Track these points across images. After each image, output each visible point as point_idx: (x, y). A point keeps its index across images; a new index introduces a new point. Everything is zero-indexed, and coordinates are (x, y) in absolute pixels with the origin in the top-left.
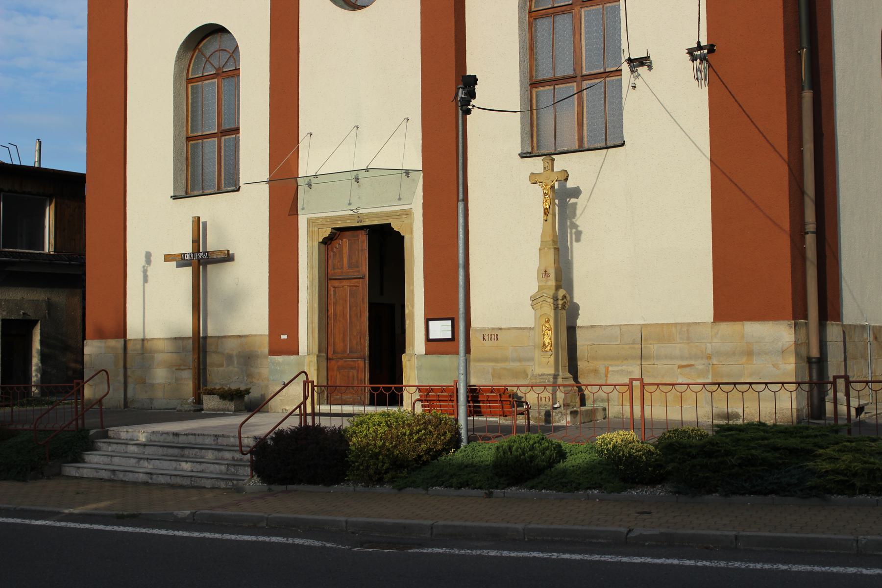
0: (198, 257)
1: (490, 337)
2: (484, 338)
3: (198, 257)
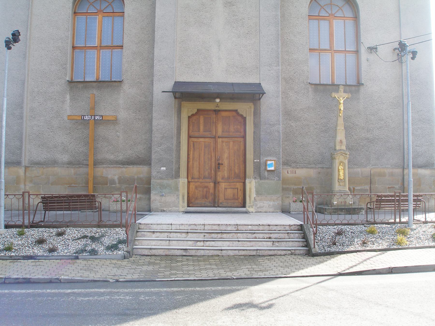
0: (94, 118)
1: (291, 172)
2: (288, 172)
3: (94, 118)
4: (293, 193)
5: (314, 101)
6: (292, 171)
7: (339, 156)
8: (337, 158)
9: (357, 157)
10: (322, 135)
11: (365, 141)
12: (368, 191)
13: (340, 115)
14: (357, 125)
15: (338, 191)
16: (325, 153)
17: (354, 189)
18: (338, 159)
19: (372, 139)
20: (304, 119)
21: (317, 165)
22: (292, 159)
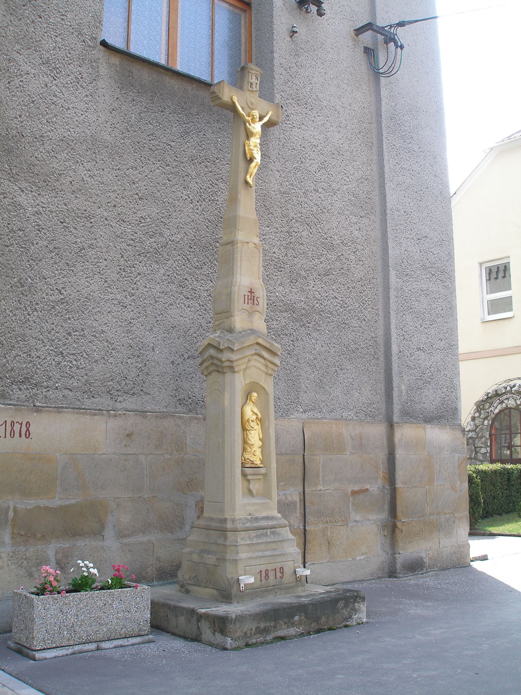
1: (9, 428)
7: (249, 361)
8: (240, 366)
10: (142, 269)
11: (285, 314)
13: (250, 180)
16: (153, 350)
18: (241, 373)
19: (303, 311)
21: (120, 399)
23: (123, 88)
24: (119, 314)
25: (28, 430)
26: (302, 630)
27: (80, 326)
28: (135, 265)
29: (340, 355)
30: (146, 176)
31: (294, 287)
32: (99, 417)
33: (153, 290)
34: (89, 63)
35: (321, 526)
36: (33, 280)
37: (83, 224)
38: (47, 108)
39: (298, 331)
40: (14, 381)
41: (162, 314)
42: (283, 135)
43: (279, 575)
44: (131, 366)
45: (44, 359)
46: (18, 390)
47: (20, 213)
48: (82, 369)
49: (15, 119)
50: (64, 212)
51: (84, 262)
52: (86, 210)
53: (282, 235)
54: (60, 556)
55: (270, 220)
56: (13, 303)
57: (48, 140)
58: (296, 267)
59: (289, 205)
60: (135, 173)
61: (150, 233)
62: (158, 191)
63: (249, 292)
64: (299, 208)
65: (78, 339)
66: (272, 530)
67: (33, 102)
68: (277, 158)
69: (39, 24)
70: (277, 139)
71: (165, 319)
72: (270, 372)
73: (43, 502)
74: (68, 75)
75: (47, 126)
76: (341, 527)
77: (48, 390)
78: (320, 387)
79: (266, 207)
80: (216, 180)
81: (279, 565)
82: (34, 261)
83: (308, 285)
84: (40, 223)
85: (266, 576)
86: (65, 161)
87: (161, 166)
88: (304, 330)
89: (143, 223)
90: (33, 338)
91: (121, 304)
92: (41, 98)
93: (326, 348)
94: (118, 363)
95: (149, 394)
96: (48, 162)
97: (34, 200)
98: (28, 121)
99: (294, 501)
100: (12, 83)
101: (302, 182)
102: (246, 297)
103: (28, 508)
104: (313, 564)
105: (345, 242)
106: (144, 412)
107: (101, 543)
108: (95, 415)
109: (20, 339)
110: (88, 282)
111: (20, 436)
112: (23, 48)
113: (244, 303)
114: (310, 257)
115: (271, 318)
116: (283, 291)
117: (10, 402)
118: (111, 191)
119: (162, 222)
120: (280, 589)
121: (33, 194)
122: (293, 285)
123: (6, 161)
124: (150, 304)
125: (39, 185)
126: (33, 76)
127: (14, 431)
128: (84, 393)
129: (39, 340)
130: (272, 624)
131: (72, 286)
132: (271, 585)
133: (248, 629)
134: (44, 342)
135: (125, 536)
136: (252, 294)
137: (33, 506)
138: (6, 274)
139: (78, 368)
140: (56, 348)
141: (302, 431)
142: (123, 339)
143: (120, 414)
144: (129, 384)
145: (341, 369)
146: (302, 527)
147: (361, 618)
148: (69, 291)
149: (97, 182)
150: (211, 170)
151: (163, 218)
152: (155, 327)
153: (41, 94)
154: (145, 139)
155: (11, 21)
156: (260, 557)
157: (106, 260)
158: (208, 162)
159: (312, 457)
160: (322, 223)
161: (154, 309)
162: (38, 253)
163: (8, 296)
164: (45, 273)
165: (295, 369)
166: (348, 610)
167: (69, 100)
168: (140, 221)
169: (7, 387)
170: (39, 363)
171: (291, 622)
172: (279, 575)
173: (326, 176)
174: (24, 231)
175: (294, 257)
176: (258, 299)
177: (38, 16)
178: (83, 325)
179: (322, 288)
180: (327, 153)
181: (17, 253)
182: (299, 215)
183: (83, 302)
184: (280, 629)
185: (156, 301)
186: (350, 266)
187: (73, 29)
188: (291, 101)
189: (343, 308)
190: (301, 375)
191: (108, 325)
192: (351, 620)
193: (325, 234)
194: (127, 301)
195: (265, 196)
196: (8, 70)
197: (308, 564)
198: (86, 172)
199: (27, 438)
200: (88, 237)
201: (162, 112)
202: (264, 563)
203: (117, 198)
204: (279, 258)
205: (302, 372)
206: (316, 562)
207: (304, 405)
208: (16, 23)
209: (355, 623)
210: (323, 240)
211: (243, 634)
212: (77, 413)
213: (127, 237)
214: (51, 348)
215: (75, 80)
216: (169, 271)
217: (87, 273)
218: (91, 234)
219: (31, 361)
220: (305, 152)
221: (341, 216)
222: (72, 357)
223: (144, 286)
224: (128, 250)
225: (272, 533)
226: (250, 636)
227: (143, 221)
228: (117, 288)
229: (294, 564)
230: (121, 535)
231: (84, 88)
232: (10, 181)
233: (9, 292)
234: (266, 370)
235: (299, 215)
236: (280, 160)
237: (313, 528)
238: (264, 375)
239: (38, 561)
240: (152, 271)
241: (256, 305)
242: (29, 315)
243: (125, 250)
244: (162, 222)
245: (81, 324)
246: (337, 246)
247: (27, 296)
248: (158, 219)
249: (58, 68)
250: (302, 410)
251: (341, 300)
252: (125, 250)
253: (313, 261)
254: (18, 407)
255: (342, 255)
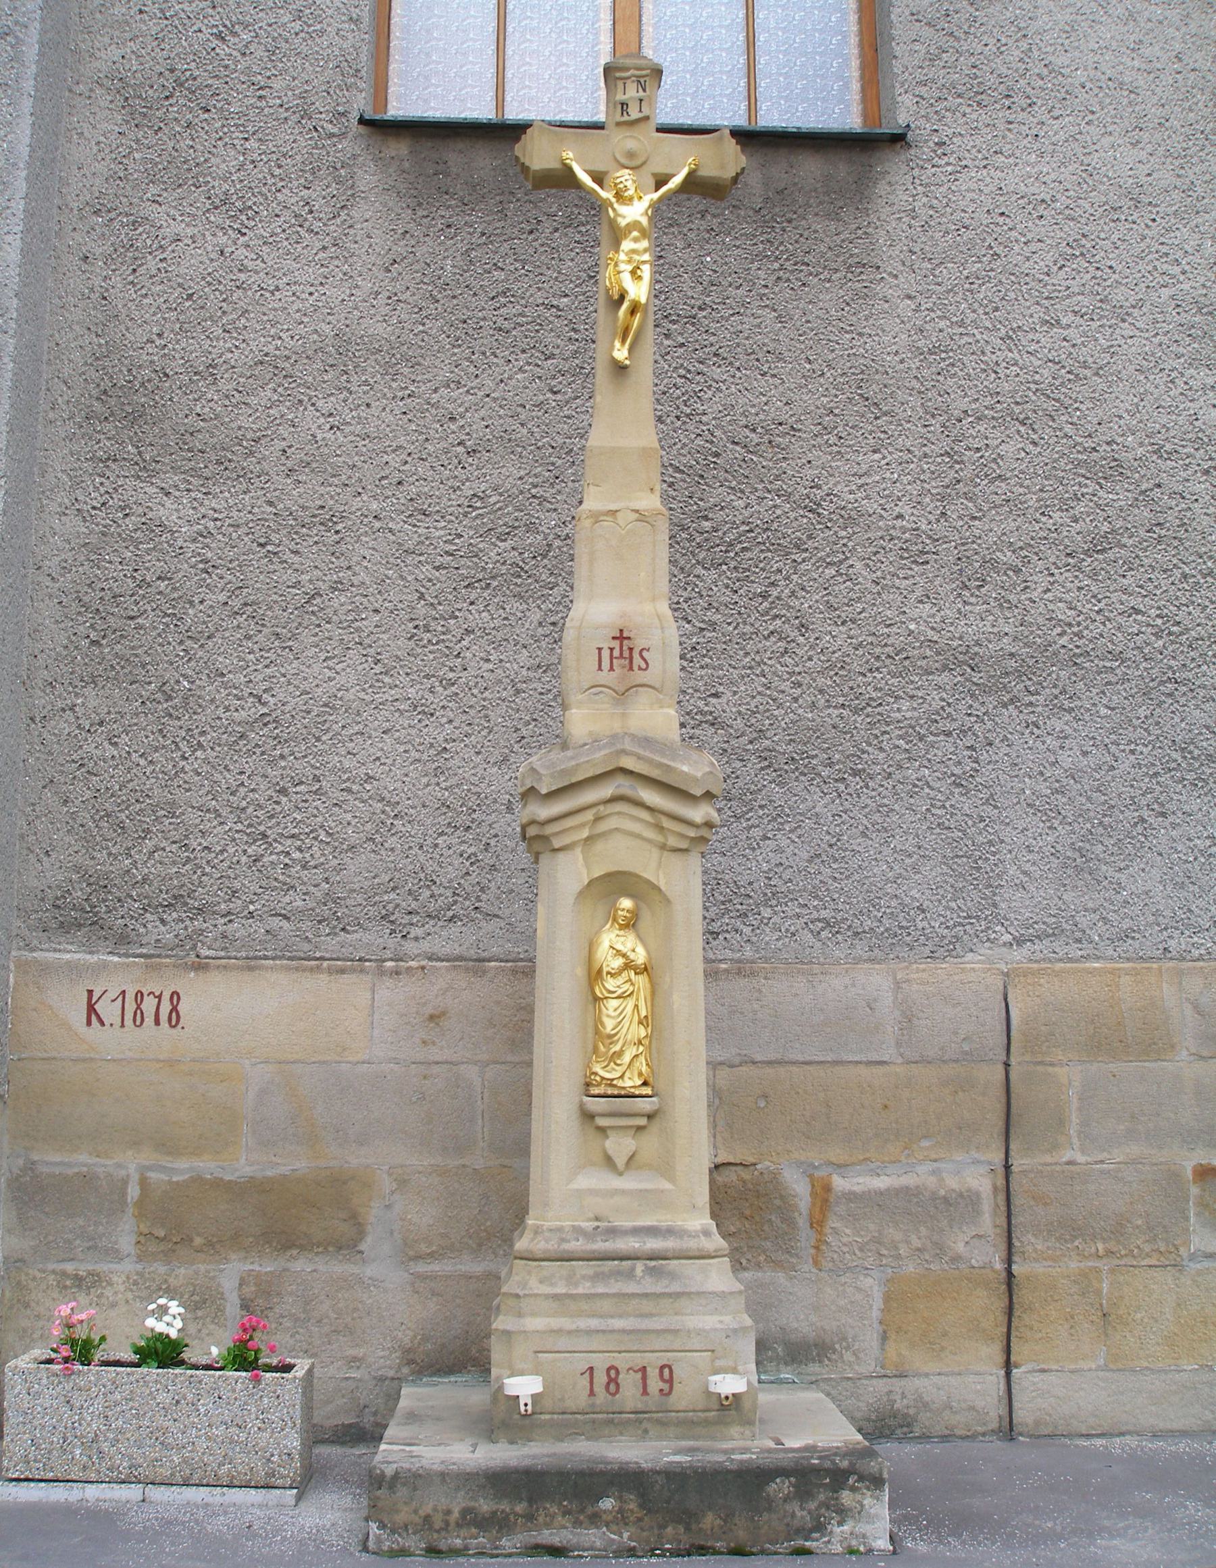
1: (130, 1007)
4: (143, 1238)
5: (399, 286)
6: (139, 996)
9: (857, 843)
11: (944, 678)
12: (978, 1212)
14: (850, 521)
15: (578, 1231)
17: (823, 1194)
20: (297, 456)
21: (416, 931)
22: (152, 869)
23: (420, 204)
24: (413, 732)
25: (174, 1009)
26: (630, 1539)
27: (309, 772)
28: (457, 613)
29: (1156, 774)
30: (488, 396)
31: (973, 600)
32: (354, 976)
33: (508, 665)
34: (330, 174)
35: (1074, 1265)
36: (193, 682)
37: (316, 539)
38: (224, 300)
39: (990, 720)
40: (149, 905)
41: (535, 720)
42: (925, 200)
43: (655, 1384)
44: (446, 852)
45: (222, 852)
46: (158, 923)
47: (161, 543)
48: (315, 867)
49: (149, 345)
50: (266, 520)
51: (319, 626)
52: (323, 507)
53: (926, 467)
54: (249, 1290)
55: (885, 432)
56: (147, 737)
57: (227, 370)
58: (979, 545)
59: (950, 382)
60: (454, 394)
61: (500, 530)
62: (522, 425)
63: (614, 638)
64: (985, 383)
65: (306, 801)
66: (653, 1263)
67: (190, 297)
68: (904, 264)
69: (204, 125)
70: (902, 215)
71: (543, 730)
72: (672, 842)
73: (207, 1166)
74: (277, 216)
75: (225, 342)
76: (1157, 1274)
77: (230, 921)
78: (1079, 870)
79: (867, 399)
80: (701, 362)
81: (654, 1361)
82: (196, 640)
83: (1026, 587)
84: (209, 555)
85: (608, 1384)
86: (271, 407)
87: (529, 364)
88: (1015, 713)
89: (477, 508)
90: (193, 807)
91: (419, 709)
92: (209, 284)
93: (1098, 756)
94: (410, 848)
95: (497, 916)
96: (227, 420)
97: (194, 508)
98: (177, 343)
99: (969, 1190)
100: (142, 270)
101: (996, 309)
102: (606, 654)
103: (174, 1179)
104: (1043, 1371)
105: (1168, 447)
106: (483, 960)
107: (355, 1269)
108: (342, 971)
109: (163, 812)
110: (330, 669)
111: (157, 1022)
112: (166, 190)
113: (600, 668)
114: (1030, 511)
115: (891, 694)
116: (933, 616)
117: (139, 951)
118: (389, 449)
119: (534, 497)
120: (659, 1422)
121: (193, 495)
122: (972, 595)
123: (131, 439)
124: (499, 699)
125: (207, 473)
126: (190, 242)
127: (142, 1013)
128: (320, 922)
129: (208, 811)
130: (520, 1508)
131: (289, 683)
132: (628, 1410)
133: (435, 1509)
134: (220, 816)
135: (418, 1257)
136: (625, 642)
137: (186, 1177)
138: (130, 677)
139: (304, 867)
140: (250, 826)
141: (1000, 997)
142: (426, 791)
143: (409, 969)
144: (440, 895)
145: (1163, 815)
146: (999, 1266)
147: (864, 1536)
148: (281, 696)
149: (352, 438)
150: (683, 341)
151: (536, 486)
152: (516, 753)
153: (209, 274)
154: (484, 309)
155: (137, 141)
156: (590, 1332)
157: (376, 611)
158: (674, 322)
159: (1040, 1068)
160: (1077, 409)
161: (512, 709)
162: (204, 623)
163: (136, 724)
164: (222, 662)
165: (982, 825)
166: (812, 1505)
167: (278, 269)
168: (469, 506)
169: (132, 917)
170: (208, 862)
171: (590, 1510)
172: (655, 1384)
173: (1089, 276)
174: (170, 579)
175: (975, 518)
176: (645, 654)
177: (202, 108)
178: (317, 768)
179: (1080, 589)
180: (1092, 211)
181: (155, 628)
182: (988, 401)
183: (318, 715)
184: (548, 1525)
185: (518, 692)
186: (1188, 514)
187: (287, 110)
188: (953, 102)
189: (1166, 638)
190: (1002, 842)
191: (383, 761)
192: (823, 1535)
193: (1090, 436)
194: (435, 701)
195: (862, 372)
196: (132, 246)
197: (1023, 1369)
198: (322, 420)
199: (174, 1027)
200: (331, 566)
201: (531, 232)
202: (601, 1348)
203: (406, 462)
204: (917, 529)
205: (1007, 833)
206: (1055, 1367)
207: (1016, 923)
208: (152, 139)
209: (837, 1548)
210: (1080, 456)
211: (420, 1521)
212: (297, 969)
213: (435, 548)
214: (239, 827)
215: (293, 221)
216: (557, 612)
217: (328, 648)
218: (338, 558)
219: (188, 860)
220: (1005, 228)
221: (1151, 377)
222: (289, 842)
223: (482, 659)
224: (437, 579)
225: (651, 1271)
226: (442, 1529)
227: (478, 504)
228: (407, 674)
229: (713, 1361)
230: (409, 1253)
231: (317, 233)
232: (139, 477)
233: (137, 715)
234: (660, 839)
235: (988, 401)
236: (915, 267)
237: (1041, 1270)
238: (655, 853)
239: (196, 1298)
240: (506, 619)
241: (640, 668)
242: (184, 758)
243: (430, 580)
244: (534, 497)
245: (312, 766)
246: (1136, 464)
247: (179, 719)
248: (522, 492)
249: (250, 207)
250: (1008, 938)
251: (1158, 616)
252: (430, 580)
253: (1044, 519)
254: (153, 960)
255: (1159, 486)
